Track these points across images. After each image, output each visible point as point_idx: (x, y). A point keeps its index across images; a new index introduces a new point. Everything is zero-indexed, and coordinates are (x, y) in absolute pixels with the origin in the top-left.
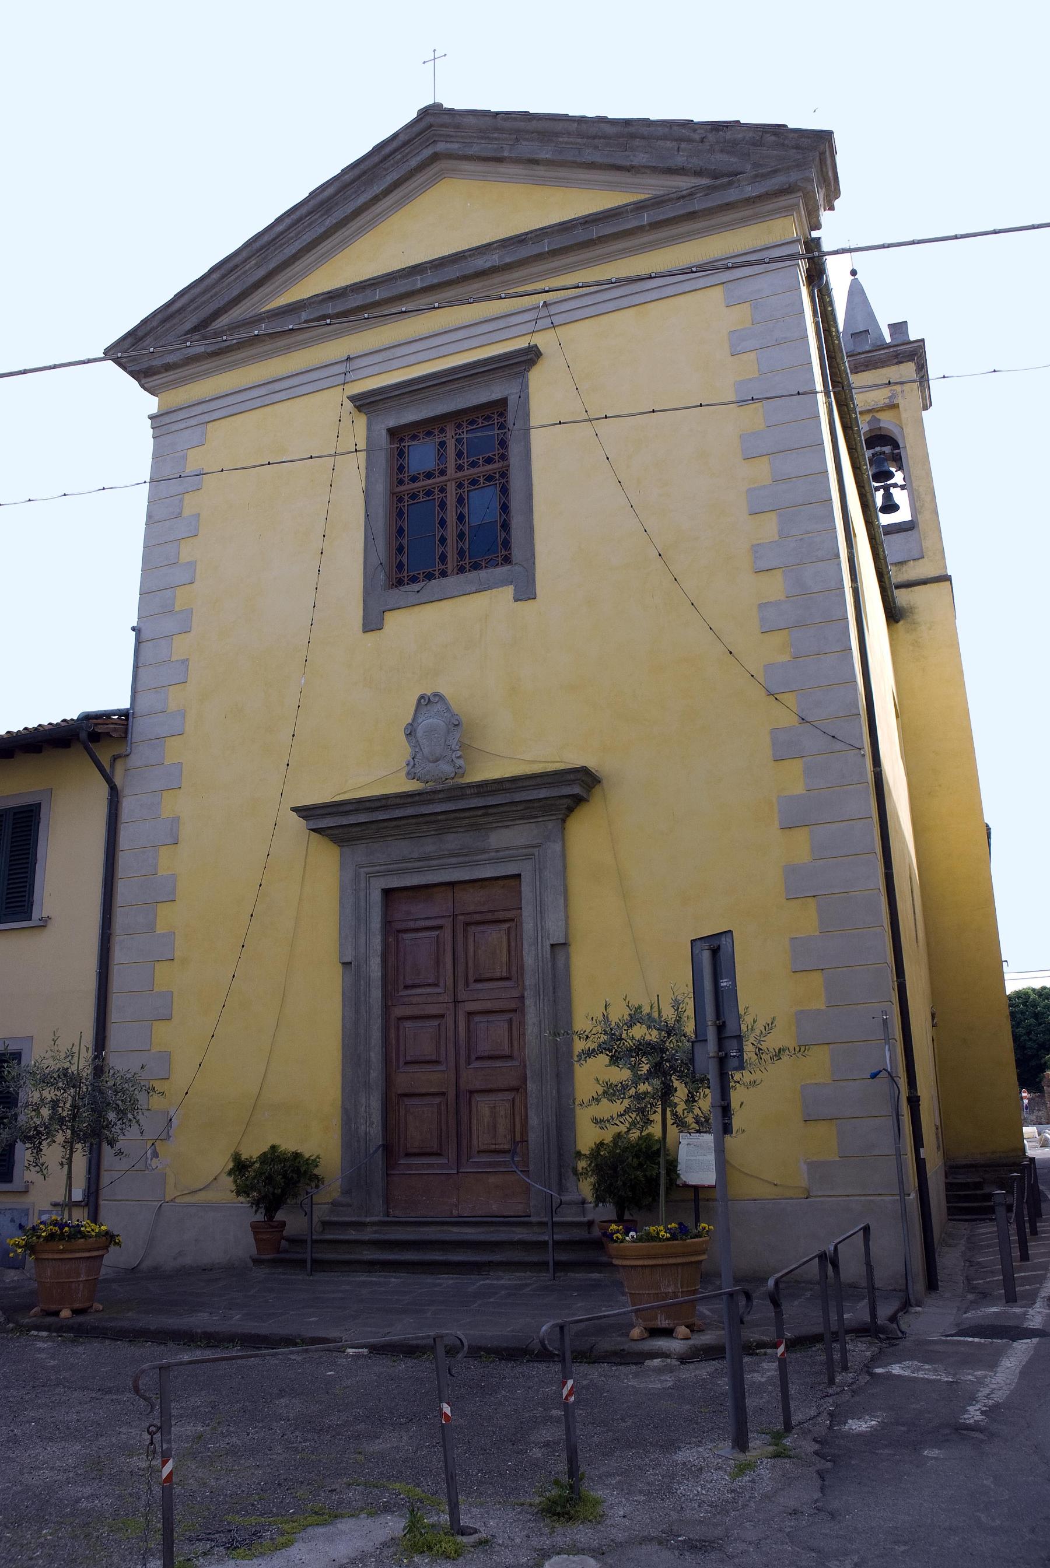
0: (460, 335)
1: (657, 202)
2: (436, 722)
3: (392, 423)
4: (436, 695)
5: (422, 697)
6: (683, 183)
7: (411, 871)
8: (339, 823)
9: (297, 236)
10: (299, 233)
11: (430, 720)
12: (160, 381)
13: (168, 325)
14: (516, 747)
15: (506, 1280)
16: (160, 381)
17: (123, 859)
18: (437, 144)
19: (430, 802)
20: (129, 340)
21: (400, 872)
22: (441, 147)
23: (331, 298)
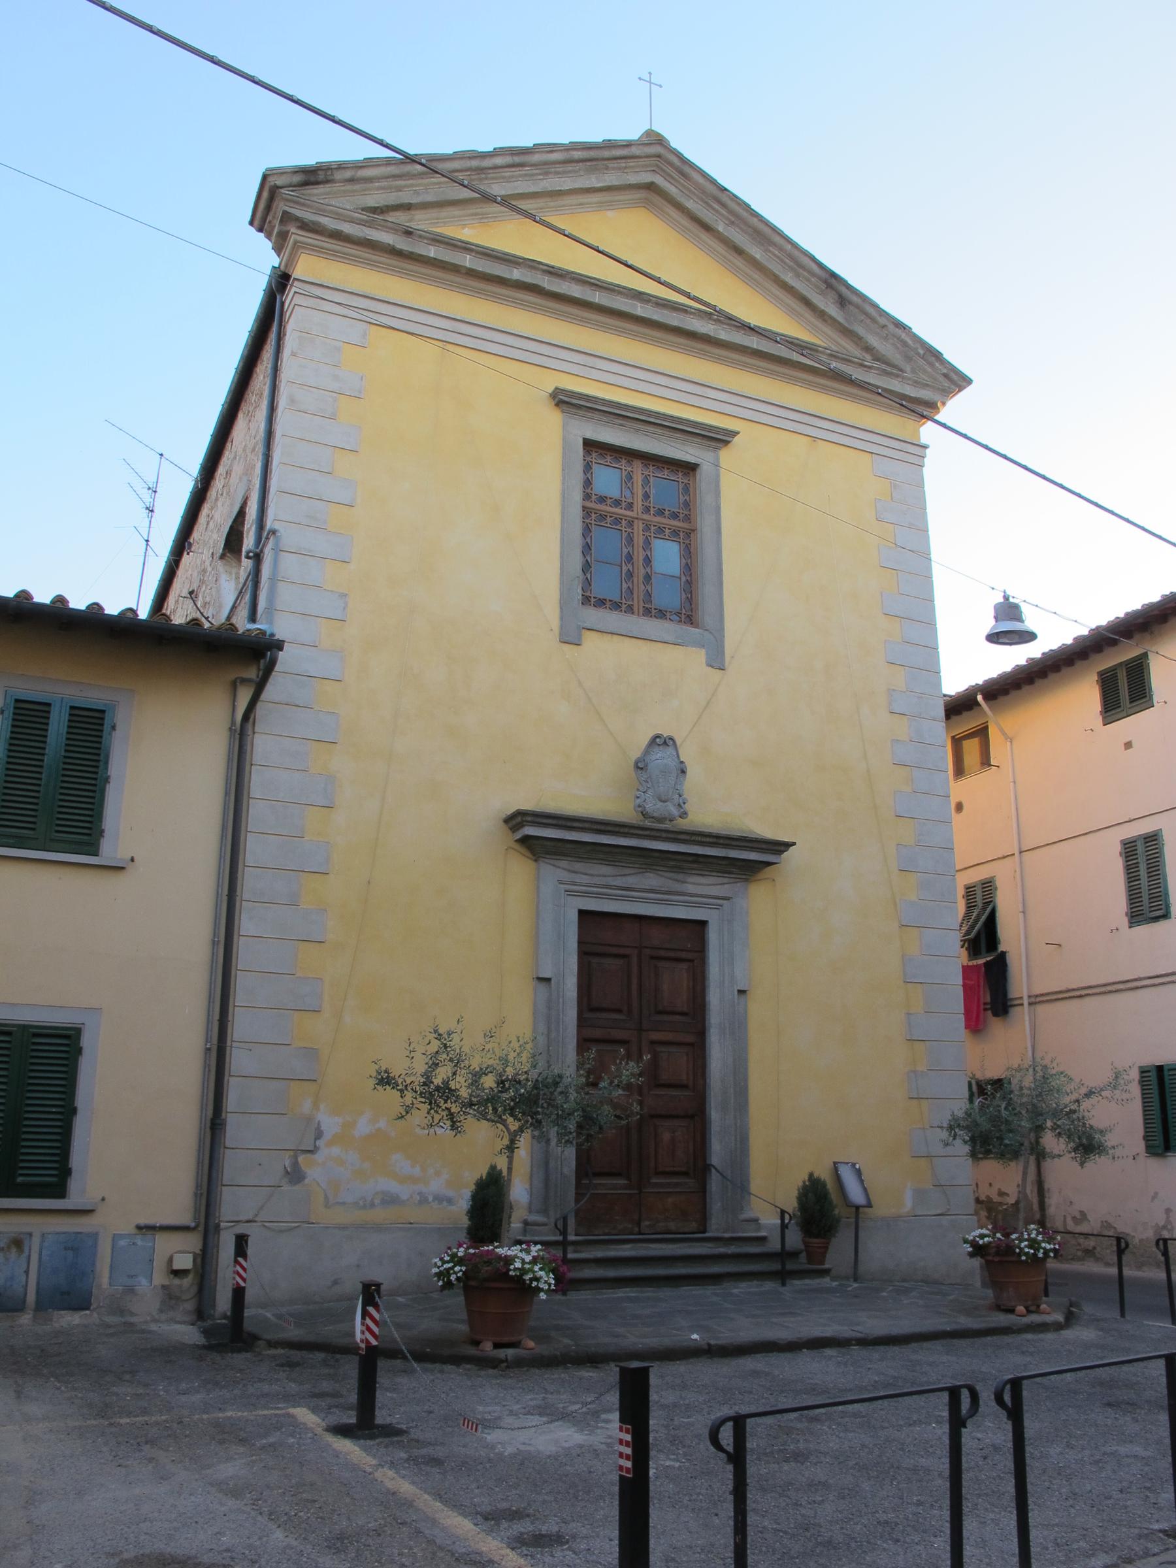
0: (896, 444)
1: (792, 343)
2: (658, 757)
3: (590, 435)
4: (671, 739)
5: (658, 736)
6: (856, 352)
7: (610, 897)
8: (539, 836)
9: (508, 180)
10: (512, 177)
11: (661, 757)
12: (310, 241)
13: (349, 187)
14: (717, 802)
15: (740, 1289)
16: (310, 241)
17: (257, 813)
18: (652, 175)
19: (655, 838)
20: (297, 179)
21: (598, 896)
22: (659, 180)
23: (550, 273)
